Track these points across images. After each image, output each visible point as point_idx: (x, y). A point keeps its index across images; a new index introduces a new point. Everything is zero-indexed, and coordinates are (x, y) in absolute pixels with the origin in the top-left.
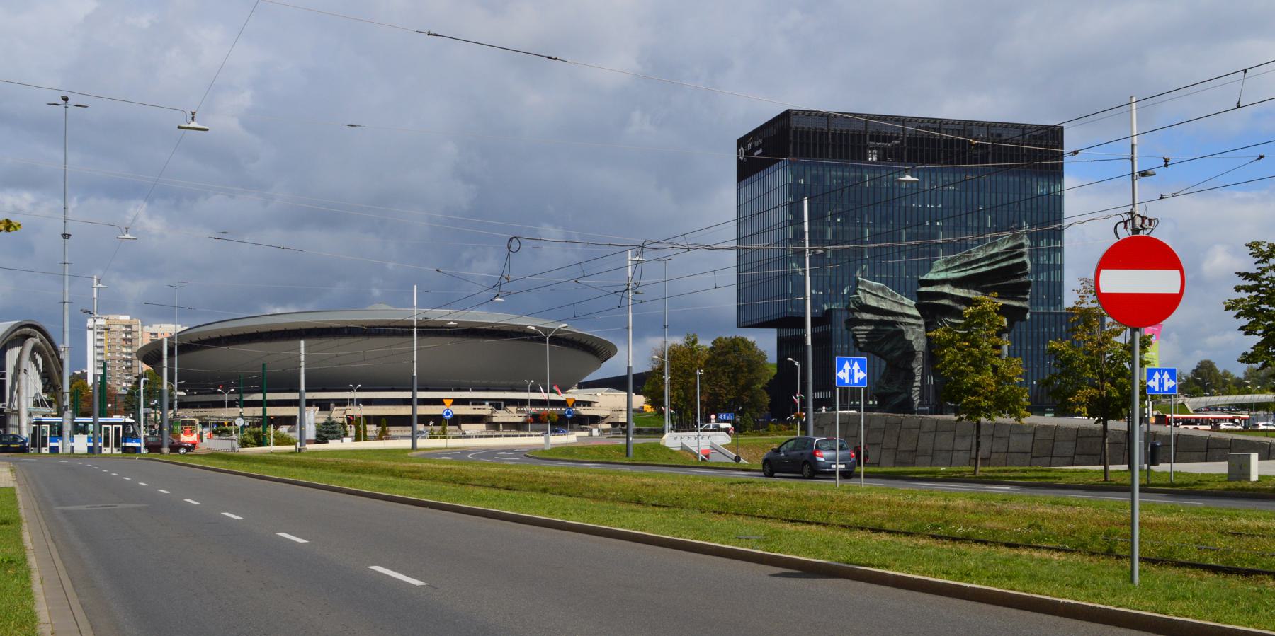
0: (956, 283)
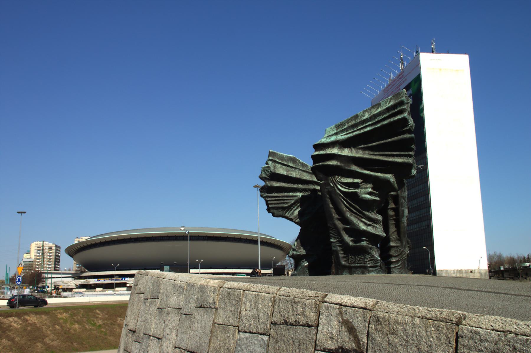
0: (343, 144)
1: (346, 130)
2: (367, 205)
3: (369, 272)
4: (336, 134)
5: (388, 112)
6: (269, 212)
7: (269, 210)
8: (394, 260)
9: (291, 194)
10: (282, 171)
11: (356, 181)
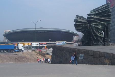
0: (95, 15)
1: (95, 11)
2: (101, 30)
3: (100, 45)
4: (93, 12)
5: (109, 14)
6: (76, 30)
7: (76, 30)
8: (106, 42)
9: (82, 26)
10: (79, 20)
11: (97, 24)
